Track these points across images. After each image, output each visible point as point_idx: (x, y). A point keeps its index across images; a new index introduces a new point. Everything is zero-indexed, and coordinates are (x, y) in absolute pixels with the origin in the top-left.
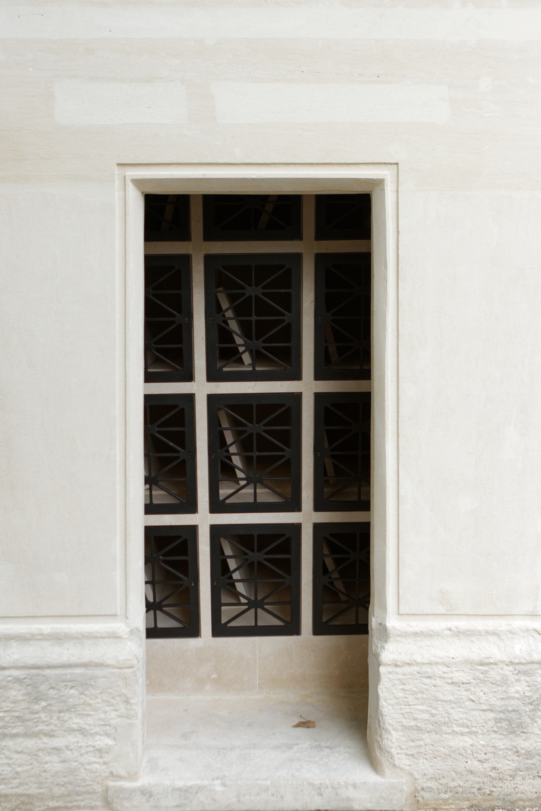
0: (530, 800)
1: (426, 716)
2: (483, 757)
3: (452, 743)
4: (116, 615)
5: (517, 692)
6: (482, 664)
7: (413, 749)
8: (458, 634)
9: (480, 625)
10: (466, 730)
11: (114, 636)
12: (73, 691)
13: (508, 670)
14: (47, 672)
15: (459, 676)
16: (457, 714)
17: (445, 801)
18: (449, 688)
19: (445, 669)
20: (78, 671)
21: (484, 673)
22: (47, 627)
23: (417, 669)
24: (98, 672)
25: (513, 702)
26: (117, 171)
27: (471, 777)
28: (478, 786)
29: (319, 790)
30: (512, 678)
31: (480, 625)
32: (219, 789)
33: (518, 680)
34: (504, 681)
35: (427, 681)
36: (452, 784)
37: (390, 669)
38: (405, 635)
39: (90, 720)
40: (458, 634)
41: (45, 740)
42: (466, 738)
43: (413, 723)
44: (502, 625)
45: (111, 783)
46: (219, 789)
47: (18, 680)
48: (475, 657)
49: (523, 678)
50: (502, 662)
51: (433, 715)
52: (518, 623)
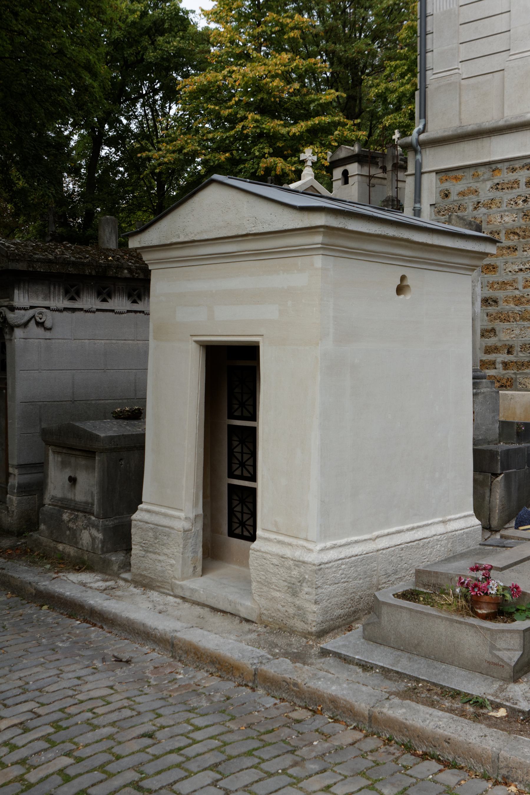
0: (300, 632)
1: (264, 578)
2: (283, 604)
3: (272, 594)
4: (182, 510)
5: (294, 575)
6: (282, 557)
7: (3, 554)
8: (279, 542)
9: (287, 540)
10: (278, 589)
11: (179, 518)
12: (165, 537)
13: (291, 563)
14: (159, 528)
15: (275, 561)
16: (274, 580)
17: (271, 622)
18: (272, 566)
19: (270, 557)
20: (167, 529)
21: (283, 562)
22: (163, 510)
23: (261, 554)
24: (172, 531)
25: (293, 579)
26: (190, 337)
27: (278, 613)
28: (281, 618)
29: (230, 602)
30: (293, 567)
31: (287, 540)
32: (202, 592)
33: (295, 569)
34: (289, 568)
35: (264, 561)
36: (273, 615)
37: (253, 552)
38: (262, 538)
39: (169, 551)
40: (279, 542)
41: (158, 556)
42: (278, 593)
43: (260, 580)
44: (294, 541)
45: (173, 580)
46: (202, 592)
47: (152, 529)
48: (281, 553)
49: (296, 568)
50: (290, 558)
51: (266, 578)
52: (301, 542)
